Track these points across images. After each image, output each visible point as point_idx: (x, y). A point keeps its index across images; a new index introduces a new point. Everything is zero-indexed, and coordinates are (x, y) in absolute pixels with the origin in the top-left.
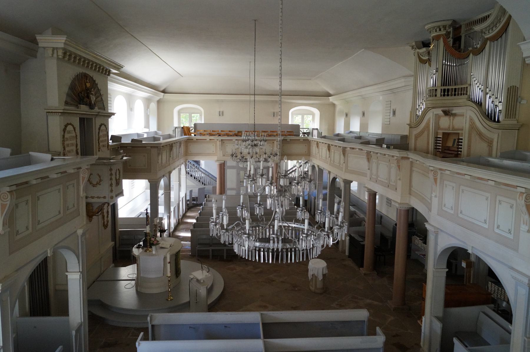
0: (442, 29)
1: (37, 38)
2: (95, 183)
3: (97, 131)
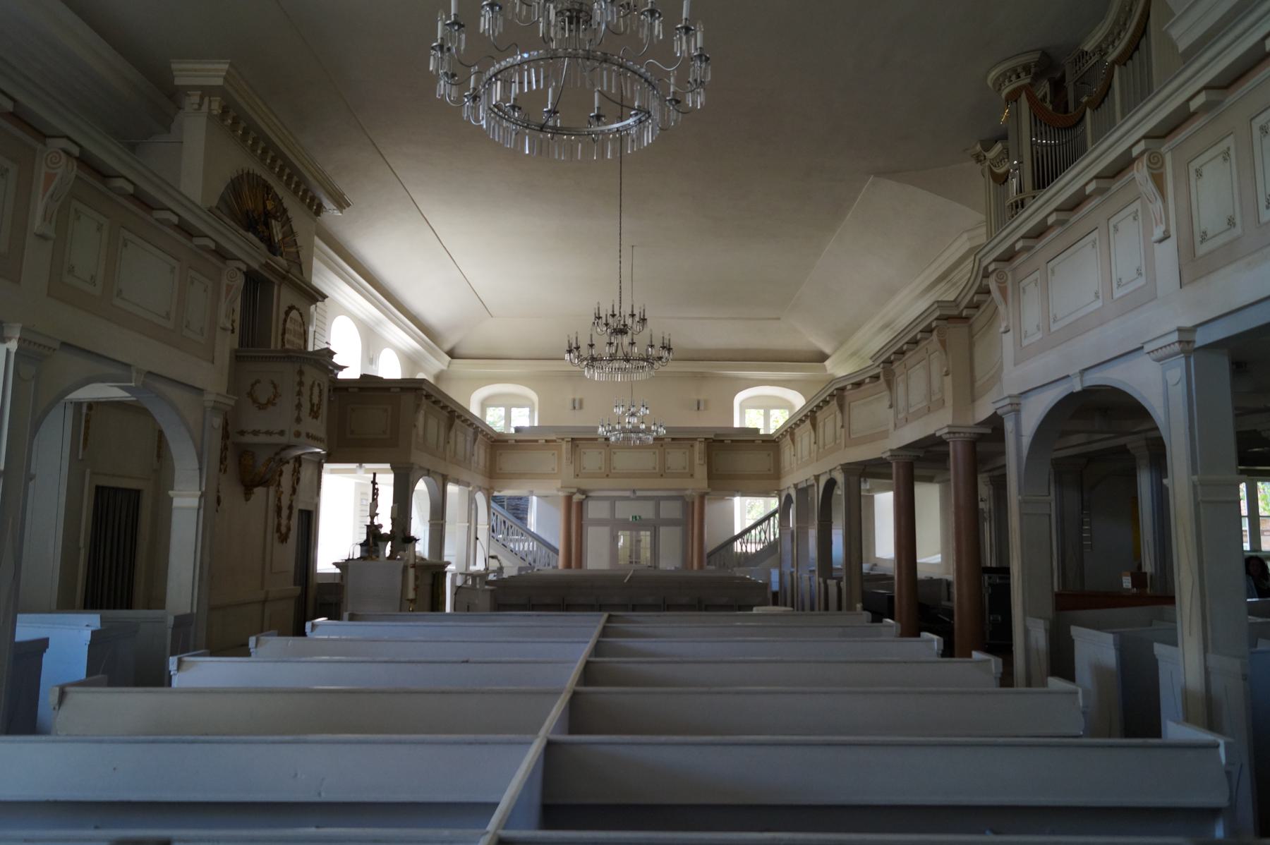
0: (1023, 75)
1: (174, 66)
2: (263, 400)
3: (282, 316)
